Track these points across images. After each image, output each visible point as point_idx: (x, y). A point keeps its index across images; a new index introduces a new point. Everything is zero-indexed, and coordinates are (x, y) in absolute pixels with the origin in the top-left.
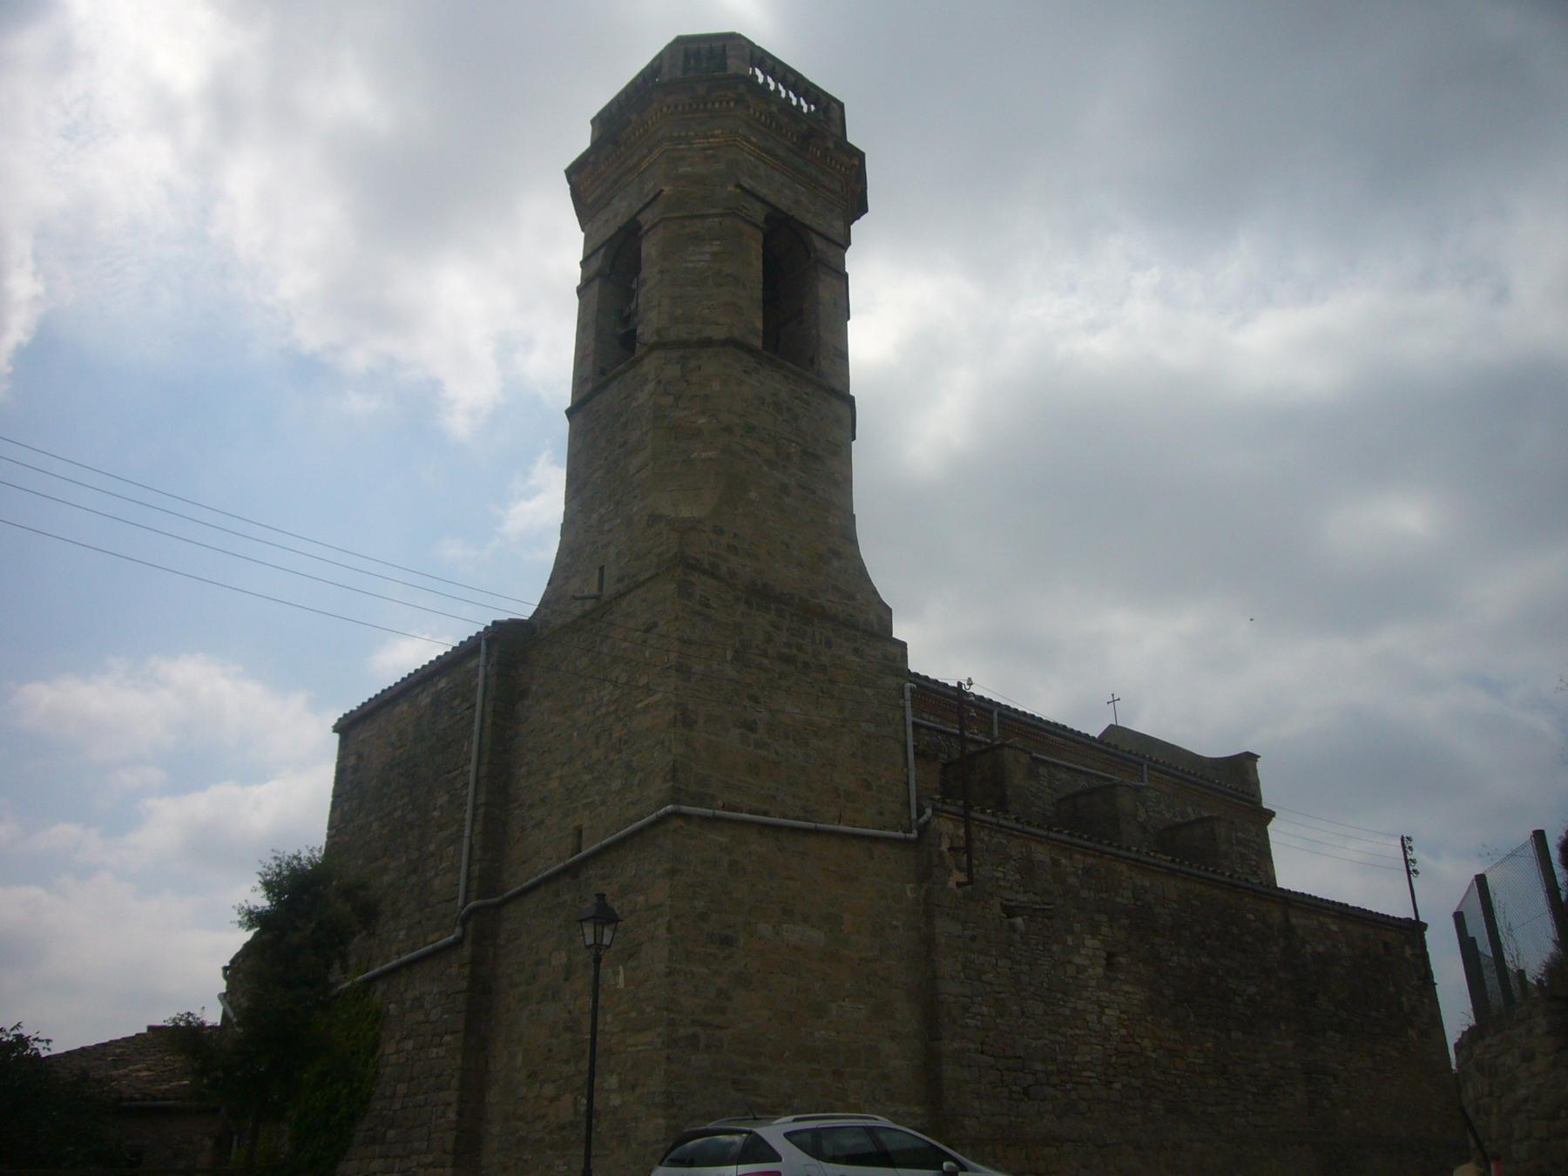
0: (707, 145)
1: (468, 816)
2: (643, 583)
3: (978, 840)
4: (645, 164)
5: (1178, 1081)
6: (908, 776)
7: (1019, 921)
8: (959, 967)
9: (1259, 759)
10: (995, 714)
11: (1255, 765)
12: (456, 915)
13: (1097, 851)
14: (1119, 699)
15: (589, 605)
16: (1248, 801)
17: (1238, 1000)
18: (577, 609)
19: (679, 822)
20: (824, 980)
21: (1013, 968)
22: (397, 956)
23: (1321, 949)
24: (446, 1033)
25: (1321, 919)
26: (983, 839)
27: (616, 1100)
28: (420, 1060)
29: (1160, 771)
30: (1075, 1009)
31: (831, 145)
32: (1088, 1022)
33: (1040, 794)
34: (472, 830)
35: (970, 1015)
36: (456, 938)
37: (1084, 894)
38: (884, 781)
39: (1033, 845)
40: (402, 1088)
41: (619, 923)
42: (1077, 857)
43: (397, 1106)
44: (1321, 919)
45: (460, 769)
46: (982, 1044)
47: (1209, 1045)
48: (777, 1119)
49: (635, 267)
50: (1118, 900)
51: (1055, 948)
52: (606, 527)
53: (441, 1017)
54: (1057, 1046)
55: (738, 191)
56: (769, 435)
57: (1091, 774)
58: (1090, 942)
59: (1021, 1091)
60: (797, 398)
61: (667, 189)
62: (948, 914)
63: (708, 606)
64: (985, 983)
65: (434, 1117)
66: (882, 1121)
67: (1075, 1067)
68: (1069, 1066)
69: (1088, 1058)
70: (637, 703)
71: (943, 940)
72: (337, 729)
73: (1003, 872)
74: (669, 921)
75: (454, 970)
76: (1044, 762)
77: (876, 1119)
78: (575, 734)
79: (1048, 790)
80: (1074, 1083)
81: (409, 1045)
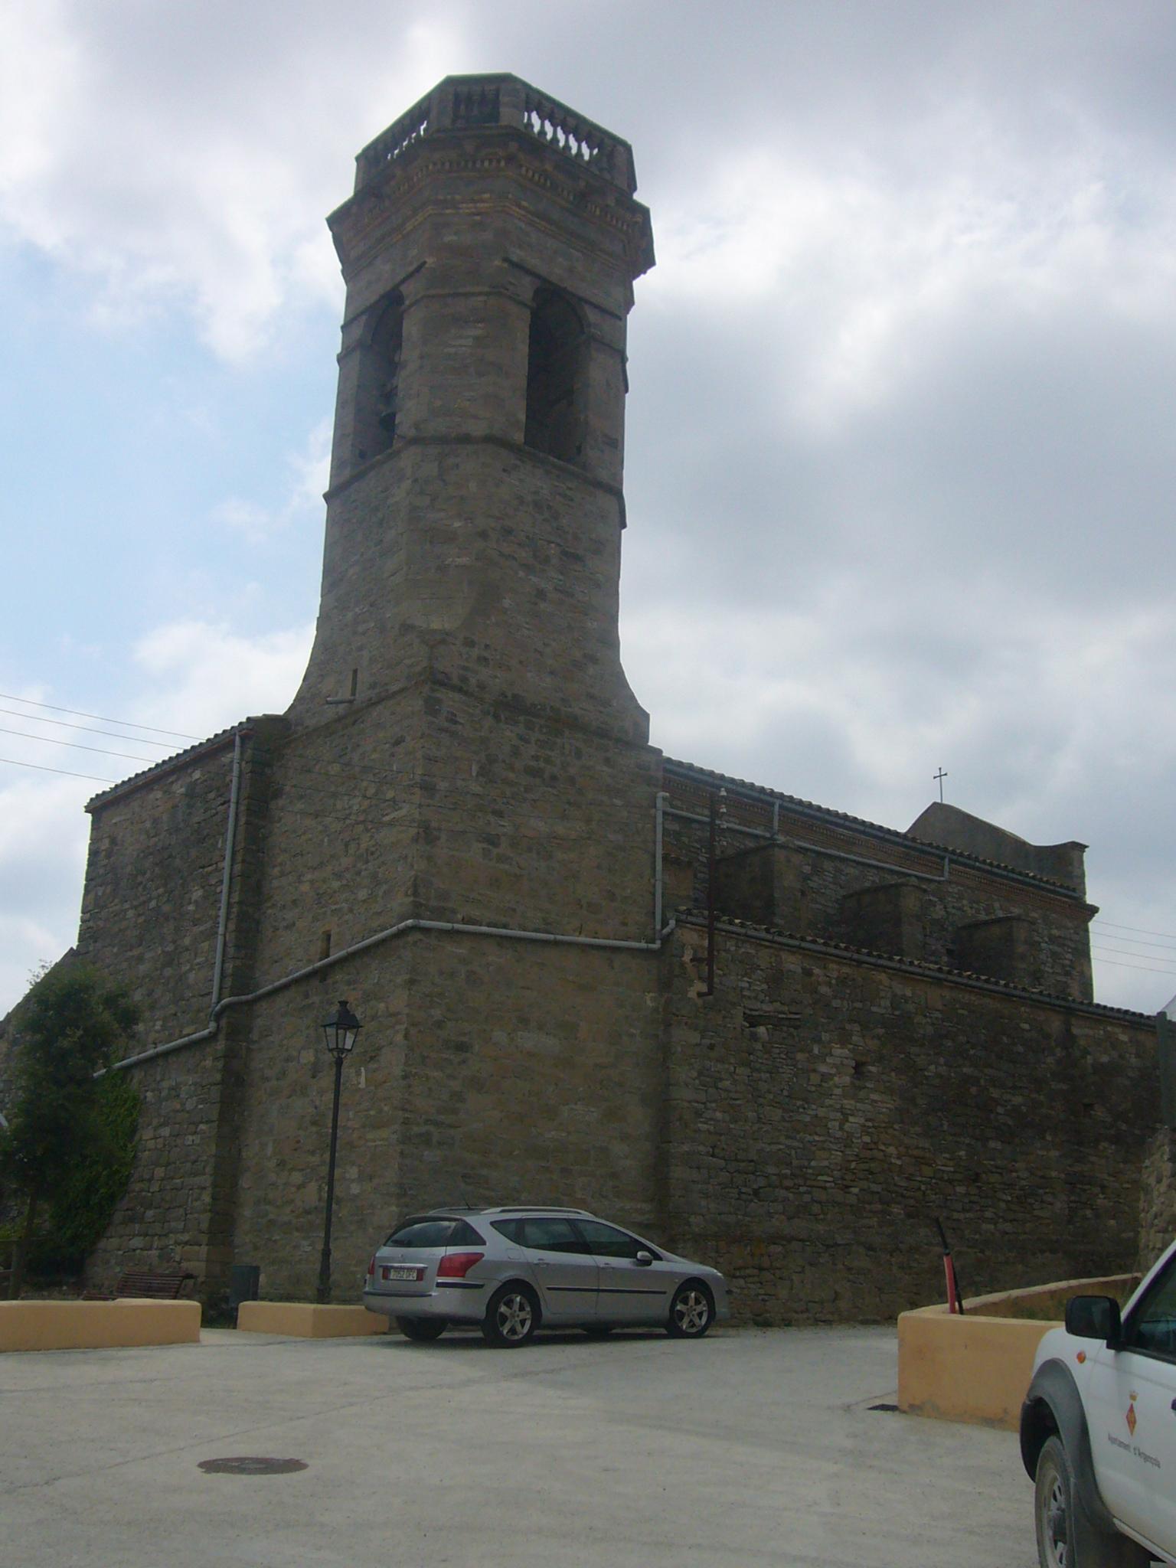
0: (473, 210)
1: (222, 912)
2: (395, 694)
3: (725, 951)
4: (409, 227)
5: (923, 1187)
6: (654, 886)
7: (761, 1030)
8: (695, 1074)
9: (1086, 849)
10: (777, 807)
11: (1082, 857)
12: (210, 1009)
13: (854, 960)
14: (946, 774)
15: (341, 709)
16: (1066, 896)
17: (1000, 1110)
18: (331, 713)
19: (419, 936)
20: (556, 1084)
21: (752, 1076)
22: (154, 1046)
23: (1105, 1059)
24: (201, 1122)
25: (1109, 1028)
26: (729, 950)
27: (355, 1189)
28: (176, 1146)
29: (965, 865)
30: (816, 1116)
31: (611, 202)
32: (829, 1129)
33: (823, 891)
34: (226, 928)
35: (702, 1120)
36: (210, 1033)
37: (836, 1003)
38: (629, 891)
39: (784, 955)
40: (160, 1172)
41: (360, 1029)
42: (831, 966)
43: (155, 1188)
44: (1109, 1028)
45: (214, 866)
46: (714, 1147)
47: (962, 1153)
48: (486, 1209)
49: (395, 340)
50: (874, 1009)
51: (800, 1056)
52: (360, 629)
53: (196, 1106)
54: (793, 1152)
55: (506, 265)
56: (528, 537)
57: (883, 869)
58: (838, 1051)
59: (751, 1193)
60: (560, 494)
61: (430, 261)
62: (686, 1024)
63: (456, 722)
64: (721, 1089)
65: (190, 1200)
66: (586, 1215)
67: (810, 1171)
68: (804, 1170)
69: (826, 1163)
70: (383, 816)
71: (679, 1049)
72: (88, 809)
73: (748, 982)
74: (406, 1029)
75: (208, 1063)
76: (830, 857)
77: (579, 1213)
78: (326, 840)
79: (831, 886)
80: (807, 1186)
81: (166, 1131)
